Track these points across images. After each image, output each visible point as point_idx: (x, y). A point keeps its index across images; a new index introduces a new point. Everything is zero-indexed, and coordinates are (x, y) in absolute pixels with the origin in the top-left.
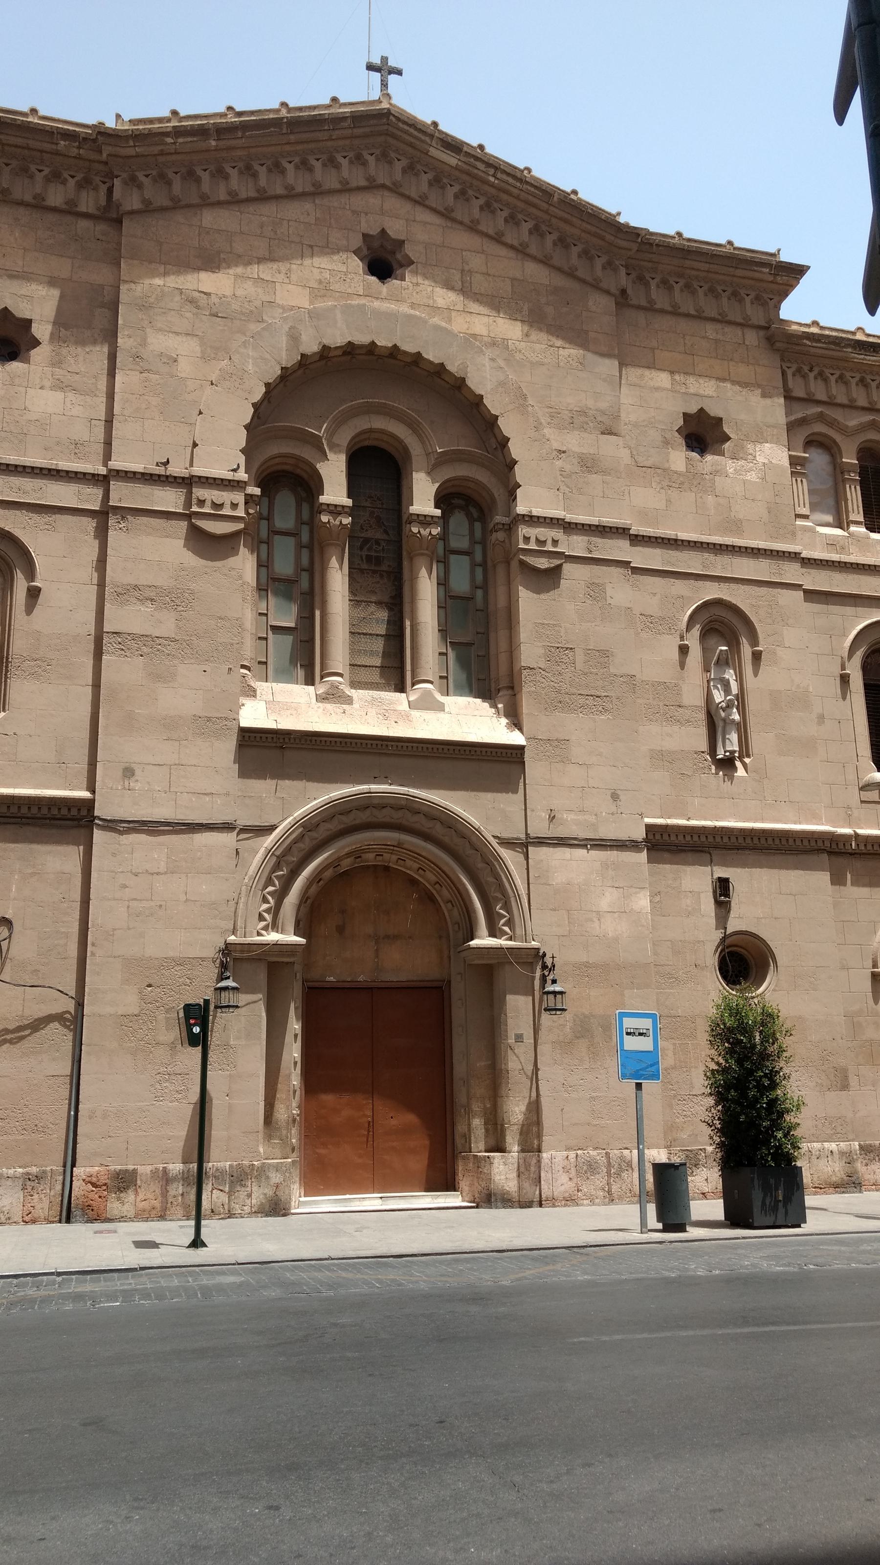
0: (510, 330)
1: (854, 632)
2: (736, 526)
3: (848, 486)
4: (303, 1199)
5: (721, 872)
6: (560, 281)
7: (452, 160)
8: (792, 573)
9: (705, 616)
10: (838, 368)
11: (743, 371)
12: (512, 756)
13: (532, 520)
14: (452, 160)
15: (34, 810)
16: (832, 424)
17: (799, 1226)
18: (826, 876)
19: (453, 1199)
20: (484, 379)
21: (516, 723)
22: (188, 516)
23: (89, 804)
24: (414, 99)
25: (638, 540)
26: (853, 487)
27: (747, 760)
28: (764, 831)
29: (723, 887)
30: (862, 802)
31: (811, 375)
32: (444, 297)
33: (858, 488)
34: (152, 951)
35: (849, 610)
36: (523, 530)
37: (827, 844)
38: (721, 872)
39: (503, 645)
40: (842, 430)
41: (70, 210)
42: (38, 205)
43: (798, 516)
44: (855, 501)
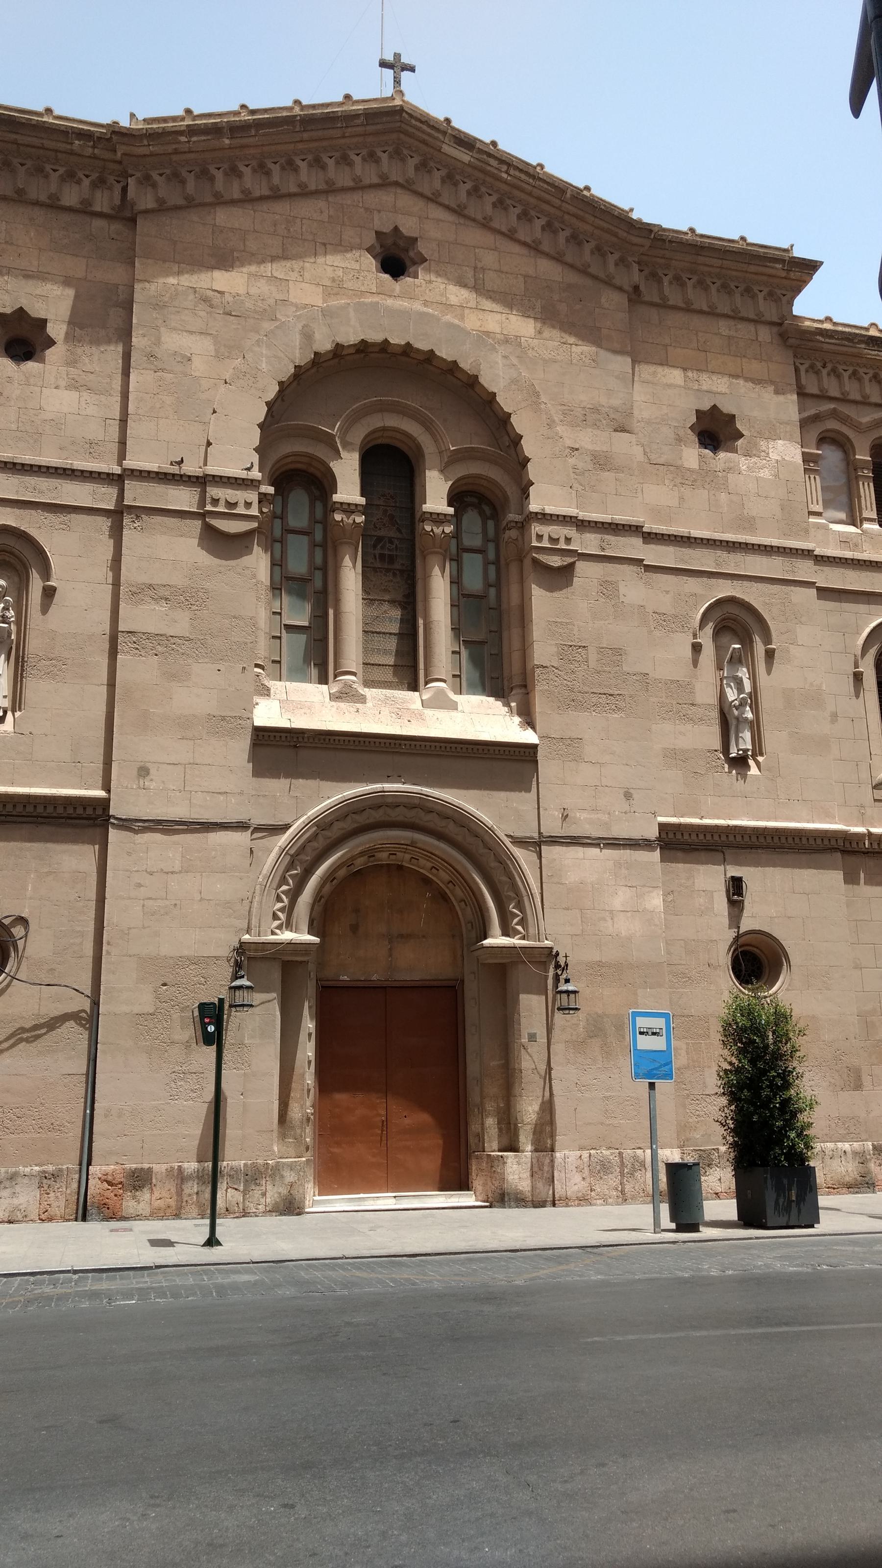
0: (523, 327)
1: (868, 630)
2: (749, 523)
3: (861, 483)
4: (317, 1198)
5: (734, 871)
6: (573, 278)
7: (465, 157)
8: (805, 570)
9: (718, 614)
10: (851, 364)
11: (755, 367)
12: (525, 755)
13: (545, 518)
14: (465, 157)
15: (50, 809)
16: (845, 420)
17: (812, 1226)
18: (839, 875)
19: (466, 1199)
20: (497, 376)
21: (529, 722)
22: (202, 516)
23: (104, 804)
24: (427, 96)
25: (651, 538)
26: (866, 484)
27: (760, 759)
28: (777, 830)
29: (736, 886)
30: (875, 800)
31: (824, 372)
32: (457, 295)
33: (871, 484)
34: (167, 949)
35: (862, 608)
36: (536, 528)
37: (841, 843)
38: (734, 871)
39: (516, 644)
40: (856, 427)
41: (85, 210)
42: (53, 205)
43: (811, 513)
44: (868, 498)
